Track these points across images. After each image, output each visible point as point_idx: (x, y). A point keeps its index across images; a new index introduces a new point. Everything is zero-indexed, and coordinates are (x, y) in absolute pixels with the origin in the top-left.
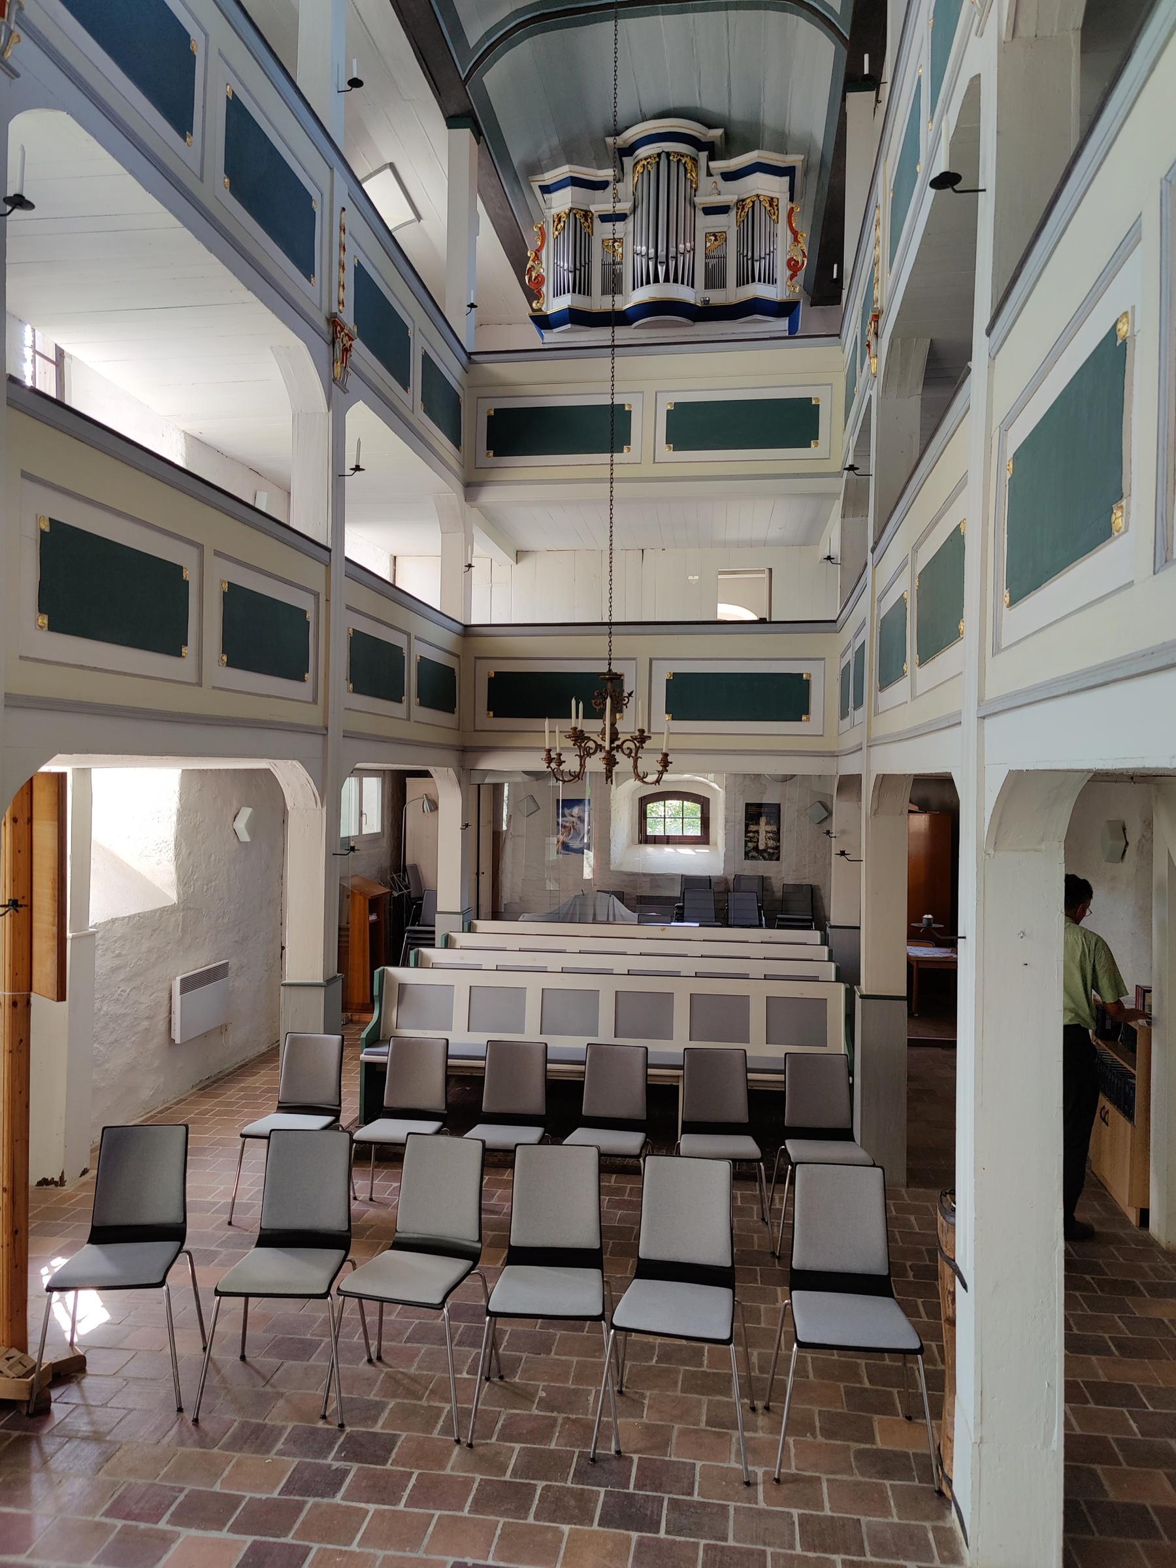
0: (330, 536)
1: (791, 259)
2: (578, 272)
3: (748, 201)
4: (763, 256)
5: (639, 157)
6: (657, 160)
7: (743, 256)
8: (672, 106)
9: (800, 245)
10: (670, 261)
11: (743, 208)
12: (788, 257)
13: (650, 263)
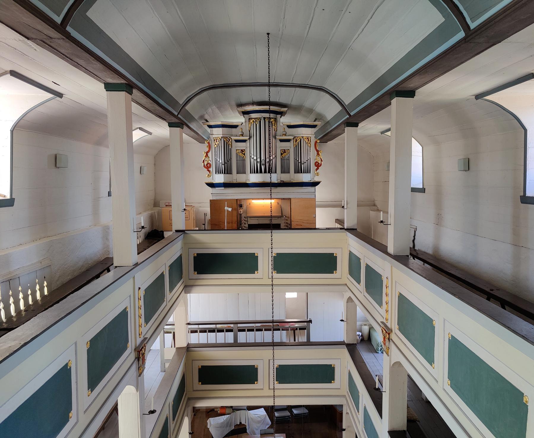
1: (317, 162)
2: (226, 164)
3: (298, 138)
4: (305, 161)
5: (252, 117)
6: (260, 120)
7: (297, 161)
8: (266, 100)
9: (320, 156)
10: (267, 164)
12: (315, 161)
13: (258, 164)
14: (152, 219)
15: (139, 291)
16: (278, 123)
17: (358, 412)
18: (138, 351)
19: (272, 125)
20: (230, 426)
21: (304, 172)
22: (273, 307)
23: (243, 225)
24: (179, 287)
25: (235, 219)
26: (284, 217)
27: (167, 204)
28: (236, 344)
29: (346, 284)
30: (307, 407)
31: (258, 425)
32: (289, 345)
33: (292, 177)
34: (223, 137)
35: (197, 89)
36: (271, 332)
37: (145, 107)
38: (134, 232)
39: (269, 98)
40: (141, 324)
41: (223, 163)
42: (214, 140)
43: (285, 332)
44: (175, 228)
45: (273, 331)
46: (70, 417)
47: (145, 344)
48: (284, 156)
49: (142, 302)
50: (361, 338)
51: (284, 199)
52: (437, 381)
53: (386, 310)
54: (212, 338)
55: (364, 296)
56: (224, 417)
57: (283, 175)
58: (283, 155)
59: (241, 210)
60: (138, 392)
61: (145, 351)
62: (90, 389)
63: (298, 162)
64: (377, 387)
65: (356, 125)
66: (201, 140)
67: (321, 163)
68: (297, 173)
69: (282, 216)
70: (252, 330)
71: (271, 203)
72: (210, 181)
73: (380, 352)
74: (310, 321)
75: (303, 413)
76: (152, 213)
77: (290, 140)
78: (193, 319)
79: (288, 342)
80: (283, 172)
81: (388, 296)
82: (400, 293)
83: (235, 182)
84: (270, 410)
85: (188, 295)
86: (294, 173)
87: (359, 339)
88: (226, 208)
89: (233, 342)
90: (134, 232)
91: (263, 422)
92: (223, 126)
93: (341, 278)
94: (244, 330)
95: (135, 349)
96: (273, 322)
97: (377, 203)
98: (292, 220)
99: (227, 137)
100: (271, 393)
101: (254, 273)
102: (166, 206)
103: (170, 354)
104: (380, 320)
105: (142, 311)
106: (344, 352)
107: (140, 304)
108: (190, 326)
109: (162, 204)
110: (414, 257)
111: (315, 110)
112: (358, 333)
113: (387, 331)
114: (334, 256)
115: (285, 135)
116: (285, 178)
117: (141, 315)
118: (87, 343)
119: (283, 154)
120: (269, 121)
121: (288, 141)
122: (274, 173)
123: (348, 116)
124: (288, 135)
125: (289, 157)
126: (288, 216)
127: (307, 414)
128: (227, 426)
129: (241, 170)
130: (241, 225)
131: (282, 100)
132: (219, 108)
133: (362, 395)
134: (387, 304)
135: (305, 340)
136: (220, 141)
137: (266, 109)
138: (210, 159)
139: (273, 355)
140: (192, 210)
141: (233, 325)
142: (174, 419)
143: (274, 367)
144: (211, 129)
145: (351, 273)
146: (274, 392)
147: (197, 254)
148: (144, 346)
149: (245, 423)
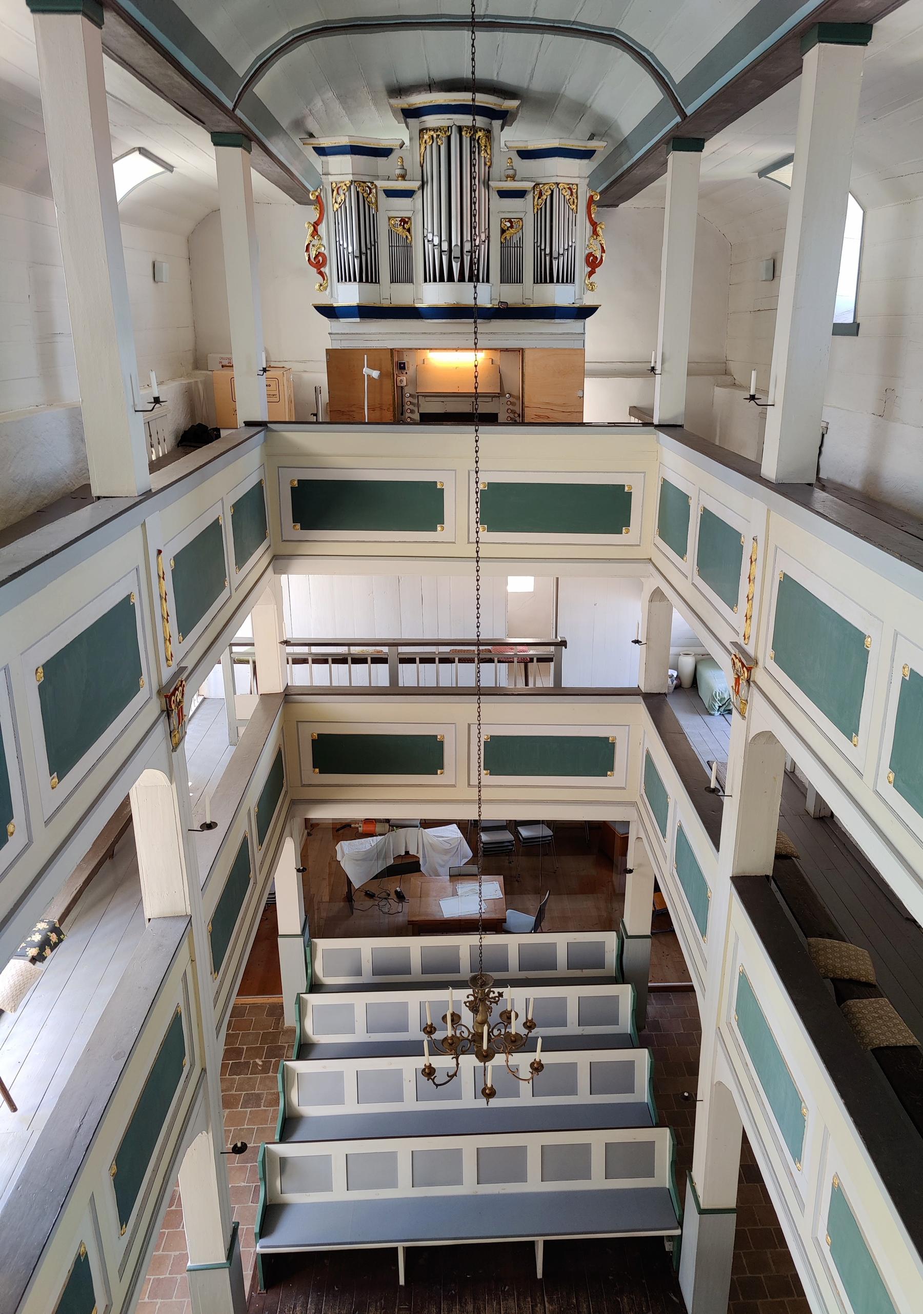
0: (188, 903)
1: (590, 254)
2: (364, 257)
3: (547, 187)
7: (541, 250)
8: (465, 77)
9: (599, 238)
10: (465, 256)
11: (541, 194)
12: (587, 252)
14: (191, 399)
15: (160, 558)
16: (495, 145)
17: (664, 836)
18: (166, 697)
19: (478, 148)
20: (385, 858)
21: (558, 281)
22: (478, 604)
23: (408, 415)
24: (259, 557)
25: (388, 399)
26: (507, 395)
27: (225, 363)
28: (394, 690)
29: (650, 559)
30: (549, 824)
31: (446, 858)
32: (513, 695)
33: (528, 294)
34: (355, 182)
35: (281, 33)
36: (472, 667)
37: (143, 77)
38: (136, 411)
39: (473, 40)
40: (170, 636)
41: (357, 253)
42: (333, 191)
43: (504, 666)
44: (243, 415)
45: (478, 663)
46: (9, 834)
47: (182, 682)
48: (508, 238)
49: (168, 585)
50: (675, 682)
51: (507, 350)
52: (861, 775)
53: (746, 616)
54: (340, 675)
55: (693, 584)
56: (372, 840)
57: (507, 287)
58: (507, 235)
59: (401, 378)
60: (174, 785)
61: (182, 697)
62: (56, 773)
63: (543, 253)
64: (712, 786)
65: (697, 145)
66: (299, 194)
67: (602, 256)
68: (541, 282)
69: (500, 395)
70: (431, 661)
71: (476, 366)
72: (325, 300)
73: (716, 712)
74: (563, 643)
75: (542, 837)
76: (191, 382)
77: (526, 191)
78: (295, 632)
79: (513, 687)
80: (506, 279)
81: (754, 583)
82: (785, 574)
83: (386, 303)
84: (470, 829)
85: (284, 577)
86: (534, 283)
87: (671, 685)
88: (366, 371)
89: (388, 685)
90: (136, 411)
91: (457, 850)
92: (355, 150)
93: (639, 545)
94: (411, 661)
95: (159, 692)
96: (478, 643)
97: (734, 367)
98: (526, 404)
99: (364, 182)
100: (473, 794)
101: (435, 530)
102: (223, 366)
103: (247, 707)
104: (728, 637)
105: (171, 606)
106: (640, 711)
107: (164, 589)
108: (290, 649)
109: (214, 360)
110: (823, 488)
111: (590, 107)
112: (671, 672)
113: (745, 663)
114: (626, 491)
115: (513, 178)
116: (512, 295)
117: (168, 615)
118: (37, 670)
119: (507, 232)
120: (471, 137)
121: (520, 194)
122: (483, 282)
123: (678, 117)
124: (520, 179)
125: (521, 240)
126: (515, 393)
127: (550, 838)
128: (378, 858)
129: (401, 275)
130: (402, 414)
131: (508, 76)
132: (343, 98)
133: (676, 802)
134: (750, 601)
135: (551, 684)
136: (347, 194)
137: (464, 100)
138: (325, 242)
139: (479, 712)
140: (285, 378)
141: (387, 647)
142: (261, 842)
143: (479, 738)
144: (323, 158)
145: (663, 532)
146: (480, 791)
147: (299, 481)
148: (181, 685)
149: (417, 853)
